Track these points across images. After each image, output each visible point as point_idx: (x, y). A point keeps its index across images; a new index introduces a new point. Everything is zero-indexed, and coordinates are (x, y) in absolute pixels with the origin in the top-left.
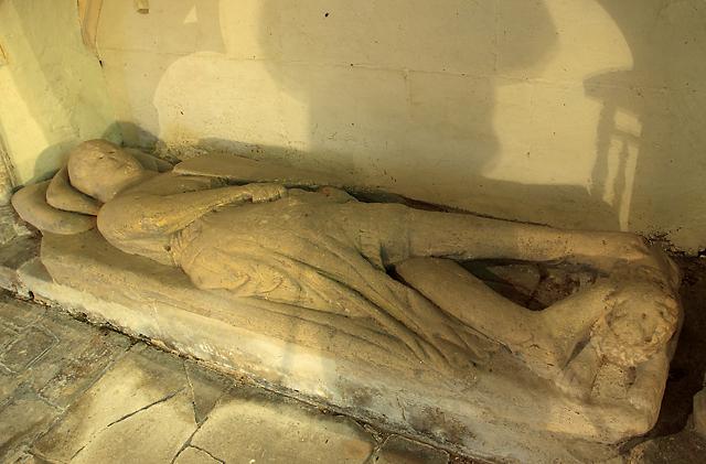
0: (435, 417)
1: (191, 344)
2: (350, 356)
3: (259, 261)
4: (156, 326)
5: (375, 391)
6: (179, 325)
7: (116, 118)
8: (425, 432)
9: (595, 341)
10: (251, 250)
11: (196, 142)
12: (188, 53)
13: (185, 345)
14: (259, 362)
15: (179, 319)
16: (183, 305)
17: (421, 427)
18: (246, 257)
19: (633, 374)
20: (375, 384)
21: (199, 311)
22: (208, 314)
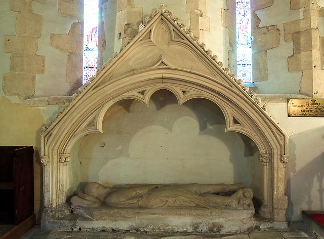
0: (214, 225)
1: (146, 227)
2: (195, 214)
3: (170, 197)
4: (134, 225)
5: (200, 223)
6: (144, 221)
7: (80, 181)
8: (212, 231)
9: (241, 201)
10: (167, 194)
11: (112, 186)
12: (116, 158)
13: (144, 228)
14: (168, 225)
15: (144, 219)
16: (147, 214)
17: (211, 229)
18: (165, 196)
19: (249, 205)
20: (200, 221)
21: (152, 214)
22: (155, 214)
